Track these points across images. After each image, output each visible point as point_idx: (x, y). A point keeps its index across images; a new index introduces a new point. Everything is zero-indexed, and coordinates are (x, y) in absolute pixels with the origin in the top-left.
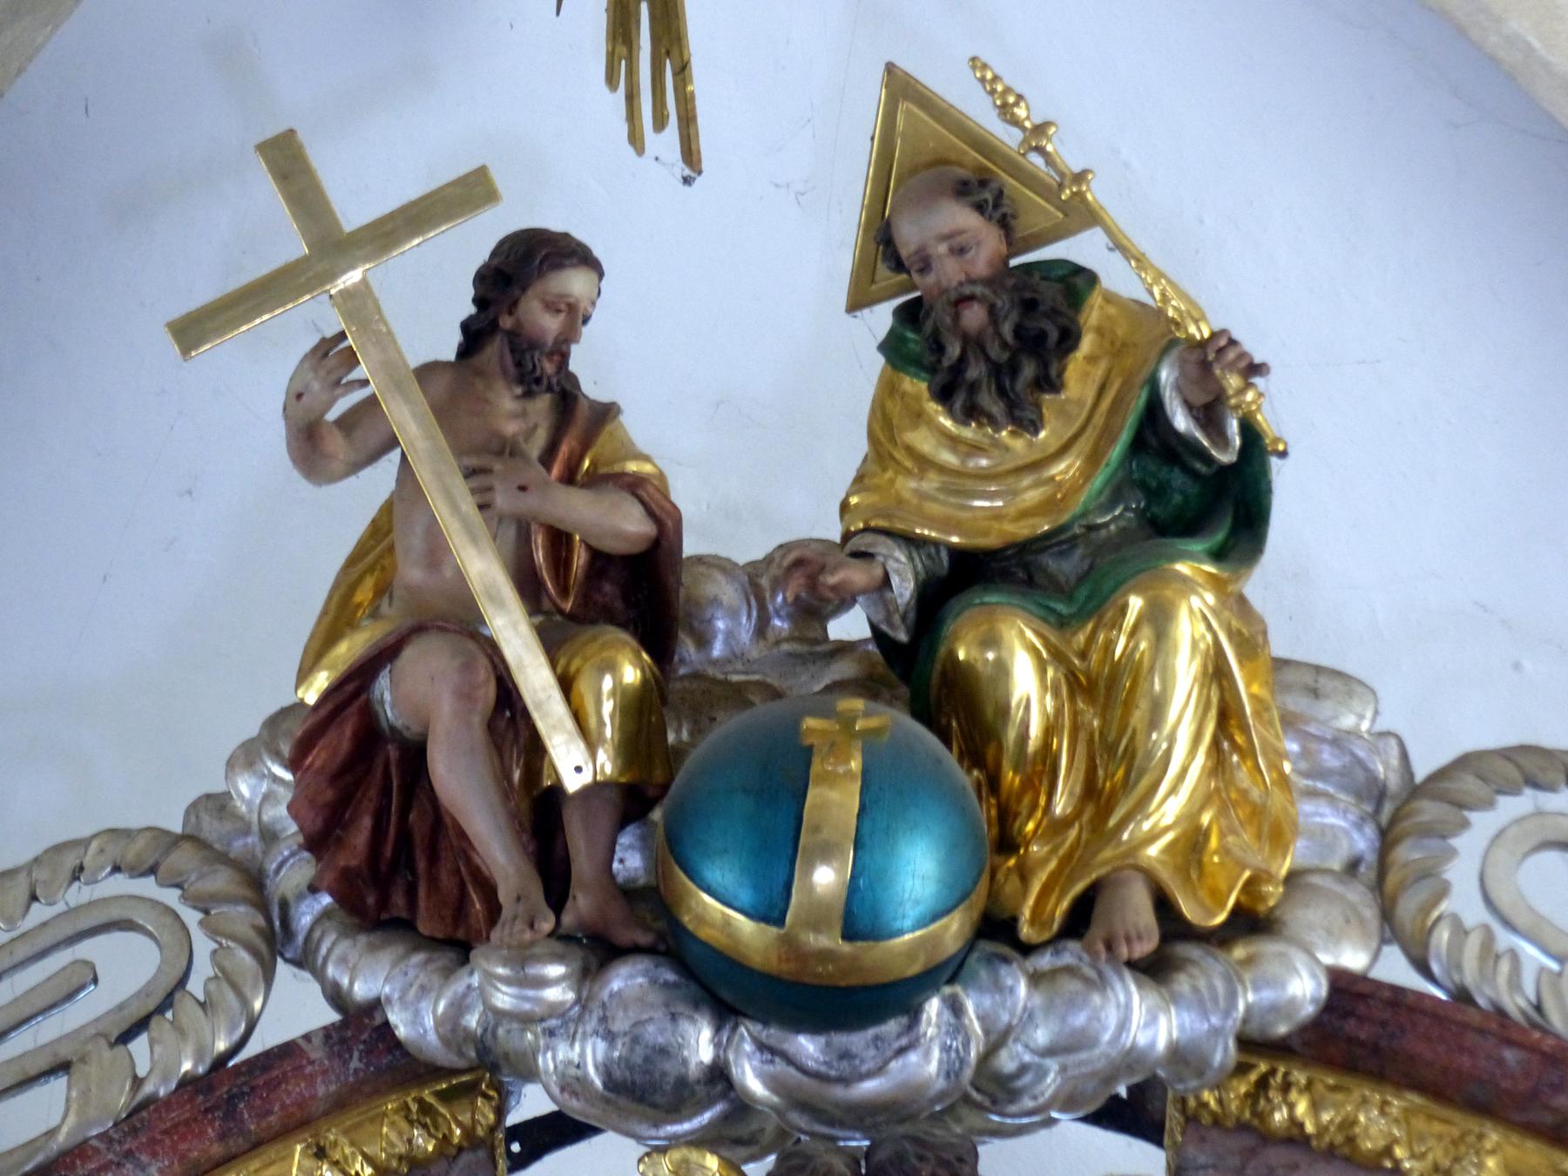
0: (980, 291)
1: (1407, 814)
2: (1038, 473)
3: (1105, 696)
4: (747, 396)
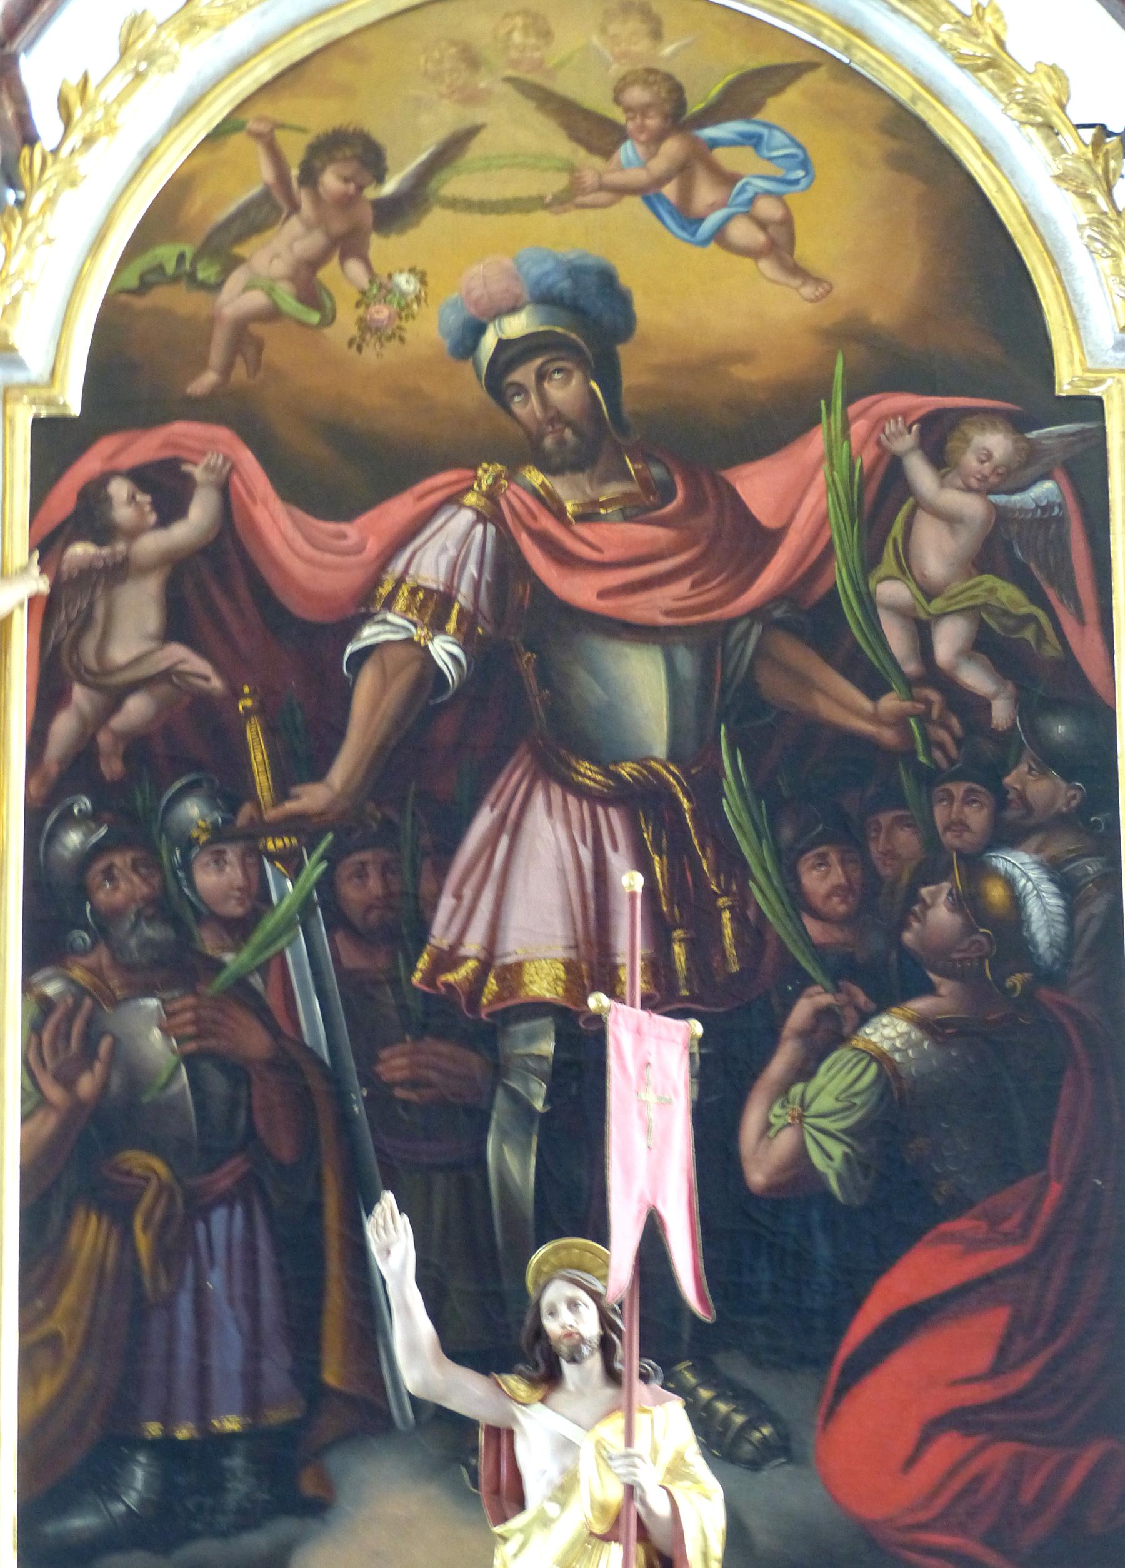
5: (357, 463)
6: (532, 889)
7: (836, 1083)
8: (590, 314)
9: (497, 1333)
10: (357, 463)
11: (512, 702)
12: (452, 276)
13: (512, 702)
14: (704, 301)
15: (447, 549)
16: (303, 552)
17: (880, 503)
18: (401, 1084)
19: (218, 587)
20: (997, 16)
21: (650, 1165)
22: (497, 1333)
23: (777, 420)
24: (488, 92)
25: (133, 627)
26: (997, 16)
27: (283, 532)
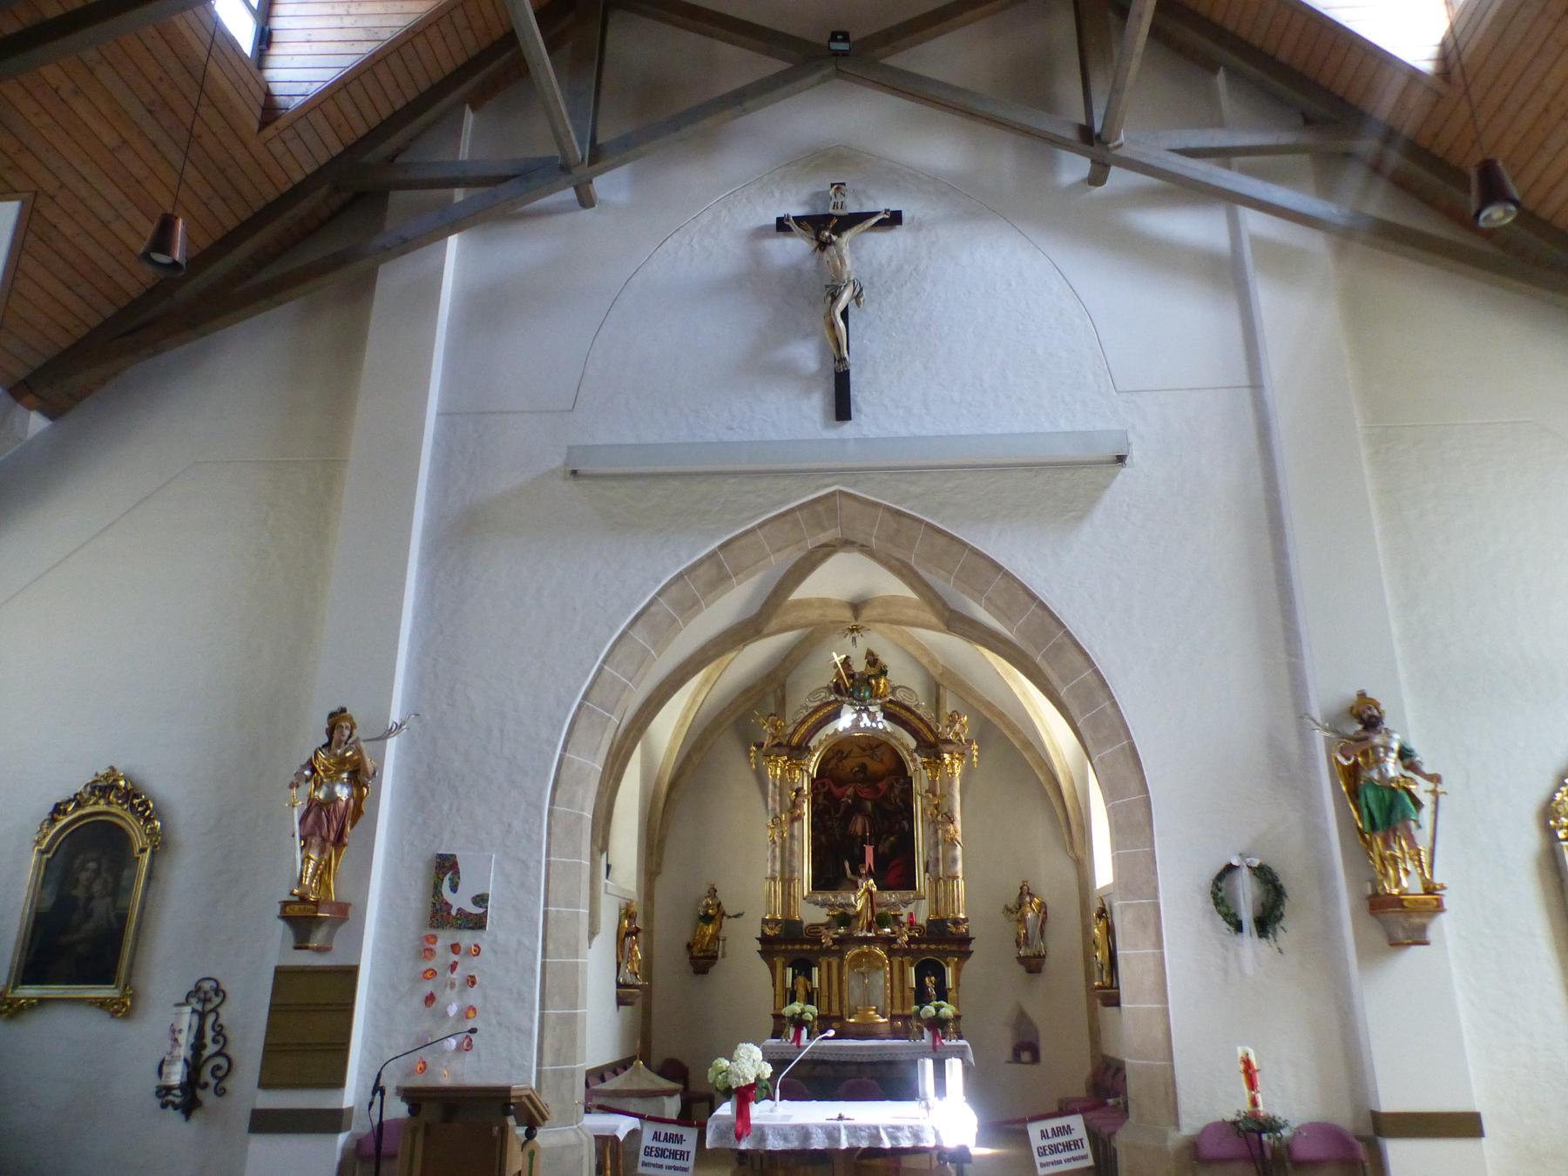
0: (872, 660)
1: (894, 689)
2: (872, 671)
3: (878, 683)
4: (859, 666)
5: (841, 783)
6: (859, 825)
7: (887, 844)
8: (863, 767)
9: (855, 871)
10: (841, 783)
11: (856, 807)
12: (850, 764)
13: (856, 807)
14: (874, 766)
15: (850, 791)
16: (837, 791)
17: (891, 787)
18: (828, 926)
19: (829, 795)
20: (471, 1014)
21: (869, 859)
22: (855, 871)
23: (880, 778)
24: (911, 915)
25: (820, 800)
26: (471, 1014)
27: (834, 789)
